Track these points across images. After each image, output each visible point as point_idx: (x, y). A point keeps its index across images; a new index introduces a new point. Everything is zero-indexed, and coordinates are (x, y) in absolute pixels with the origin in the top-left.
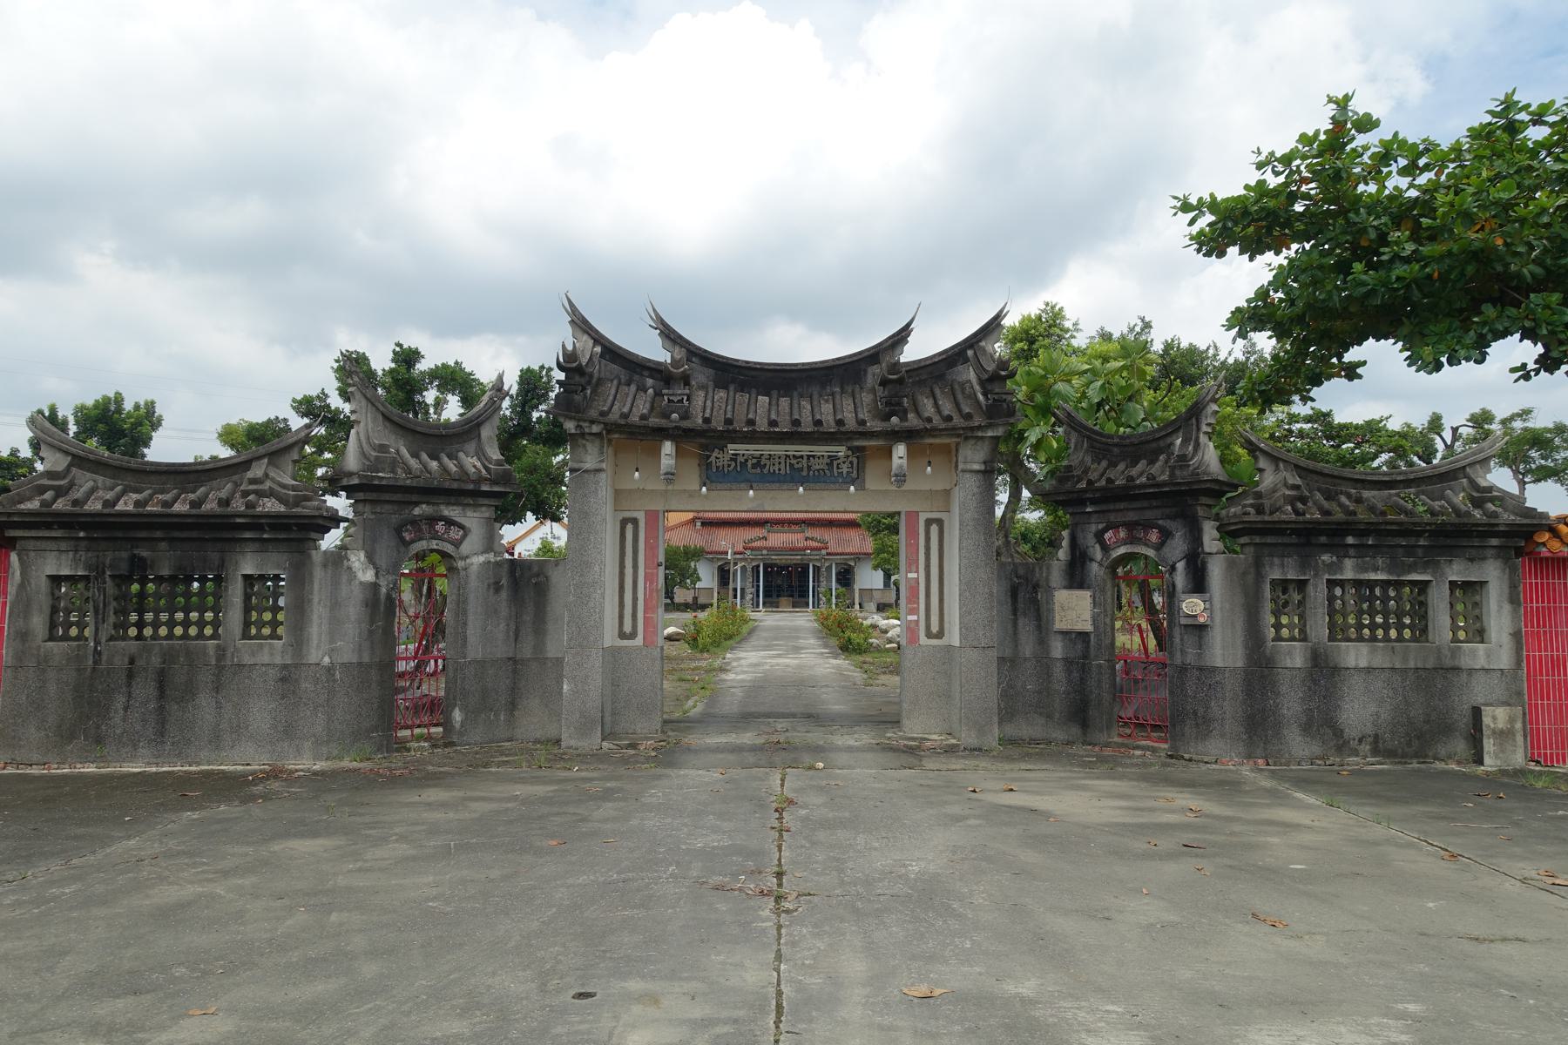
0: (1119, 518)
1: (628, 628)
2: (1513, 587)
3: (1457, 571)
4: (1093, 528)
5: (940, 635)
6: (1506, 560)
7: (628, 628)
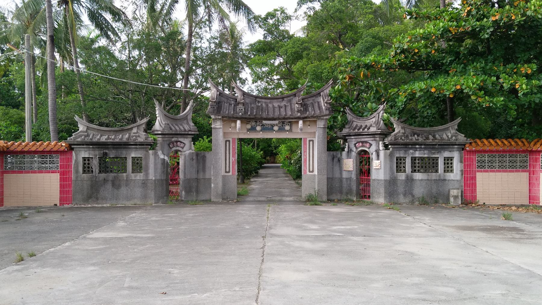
0: (360, 140)
1: (228, 170)
2: (461, 158)
3: (447, 154)
4: (354, 143)
5: (313, 171)
6: (459, 151)
7: (228, 170)
